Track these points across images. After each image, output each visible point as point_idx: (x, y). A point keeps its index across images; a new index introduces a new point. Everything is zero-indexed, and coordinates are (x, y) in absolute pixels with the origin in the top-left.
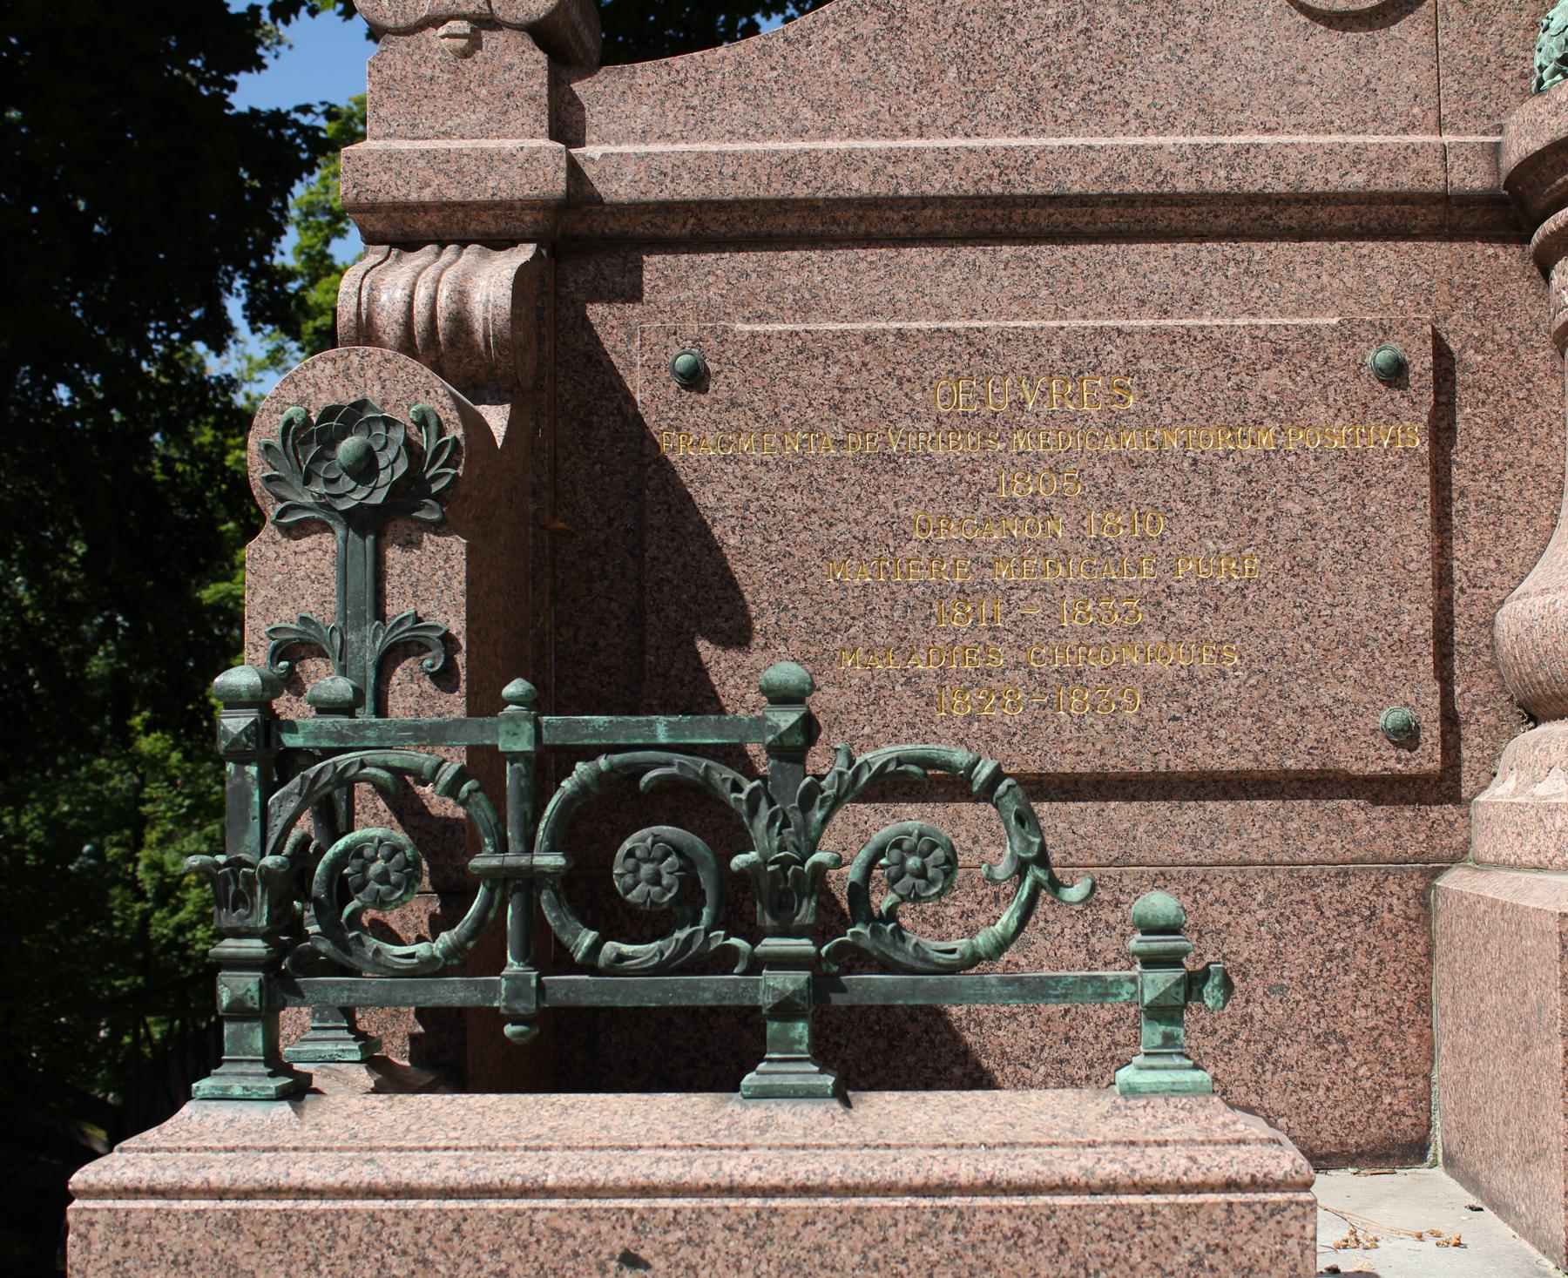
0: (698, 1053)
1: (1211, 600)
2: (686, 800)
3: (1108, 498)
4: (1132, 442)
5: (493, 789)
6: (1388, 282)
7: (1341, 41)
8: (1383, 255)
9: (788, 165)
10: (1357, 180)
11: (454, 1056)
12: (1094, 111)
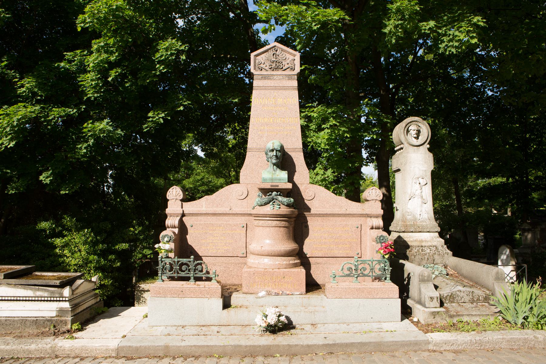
0: (187, 279)
2: (186, 264)
4: (224, 232)
5: (175, 263)
6: (243, 220)
8: (243, 218)
10: (291, 233)
11: (172, 279)
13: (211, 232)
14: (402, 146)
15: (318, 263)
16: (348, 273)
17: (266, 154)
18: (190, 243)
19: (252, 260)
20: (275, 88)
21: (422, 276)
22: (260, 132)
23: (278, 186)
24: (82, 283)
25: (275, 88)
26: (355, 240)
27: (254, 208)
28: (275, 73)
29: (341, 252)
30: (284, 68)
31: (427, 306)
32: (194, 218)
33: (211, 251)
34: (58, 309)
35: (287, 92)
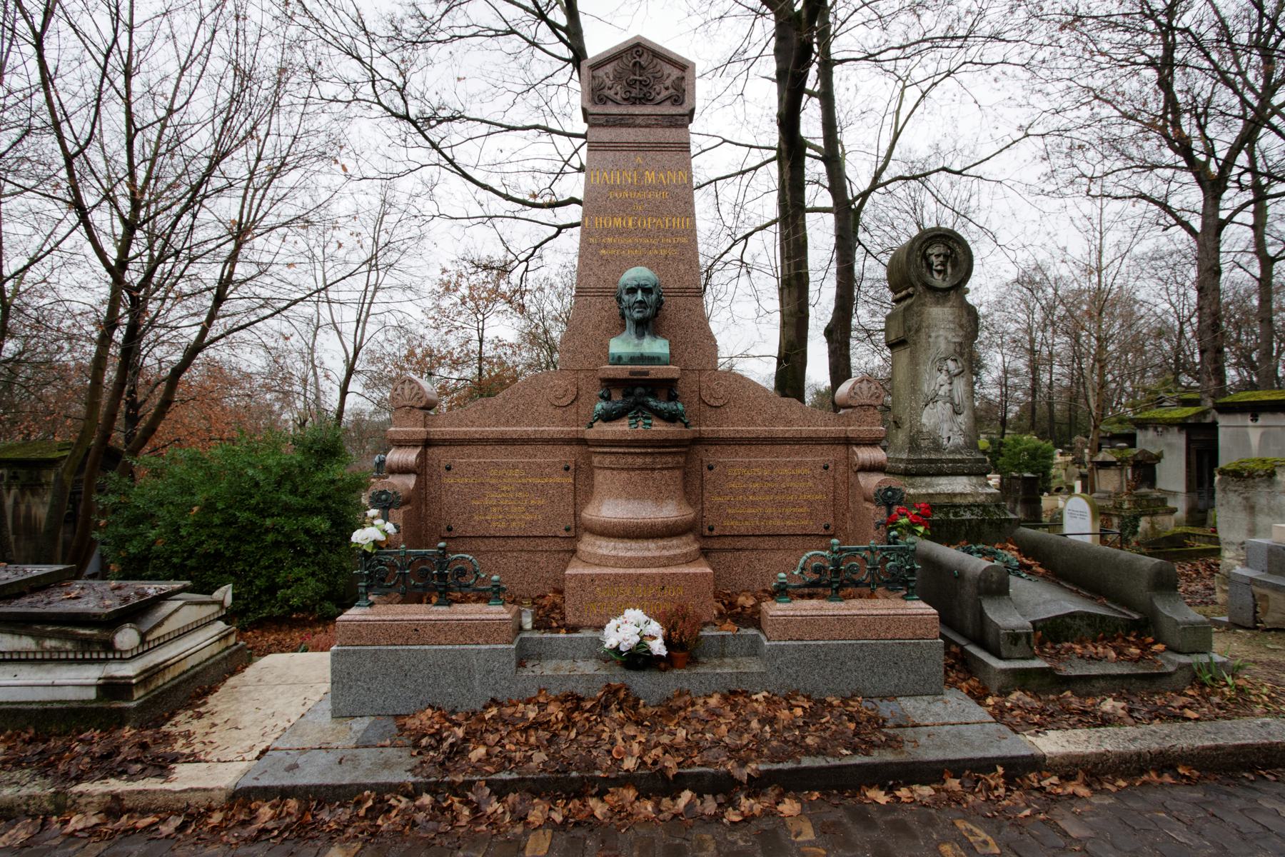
1: (537, 507)
3: (520, 490)
4: (524, 481)
7: (559, 411)
9: (465, 433)
12: (518, 423)
13: (493, 481)
14: (910, 290)
15: (738, 550)
16: (816, 577)
17: (620, 300)
18: (830, 317)
19: (592, 546)
20: (638, 147)
21: (985, 581)
22: (603, 252)
23: (647, 373)
24: (176, 611)
25: (638, 147)
26: (820, 497)
27: (591, 425)
28: (637, 110)
29: (788, 523)
30: (659, 98)
31: (1004, 654)
32: (454, 450)
33: (494, 524)
34: (101, 682)
35: (667, 155)
